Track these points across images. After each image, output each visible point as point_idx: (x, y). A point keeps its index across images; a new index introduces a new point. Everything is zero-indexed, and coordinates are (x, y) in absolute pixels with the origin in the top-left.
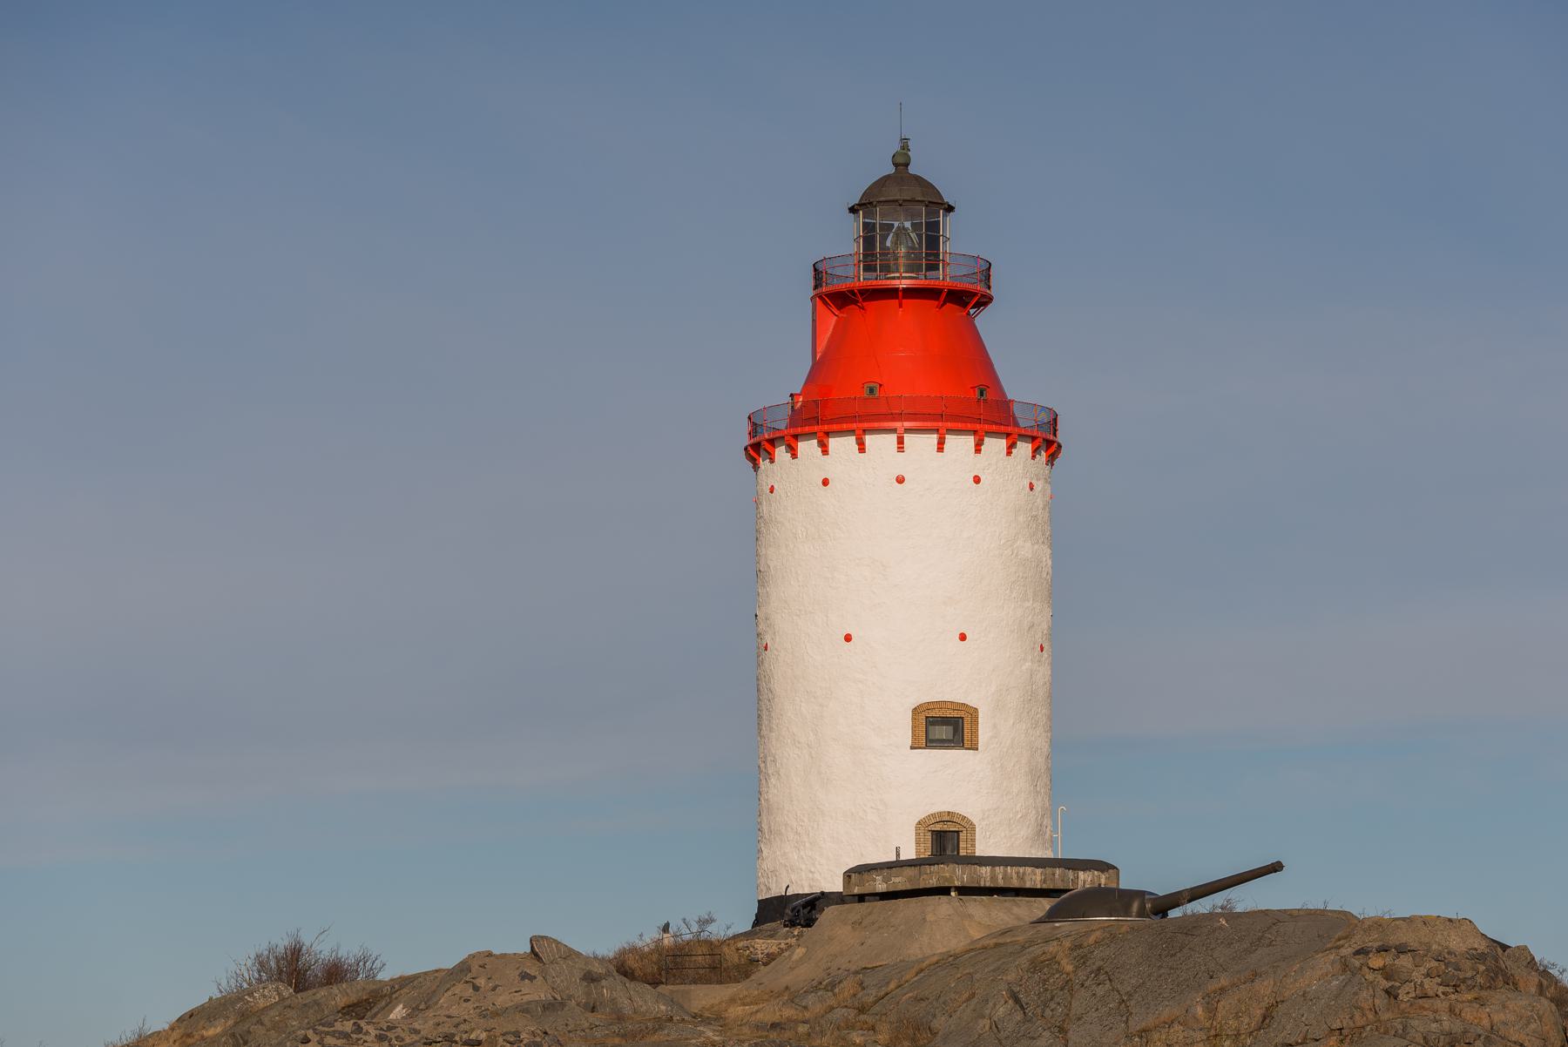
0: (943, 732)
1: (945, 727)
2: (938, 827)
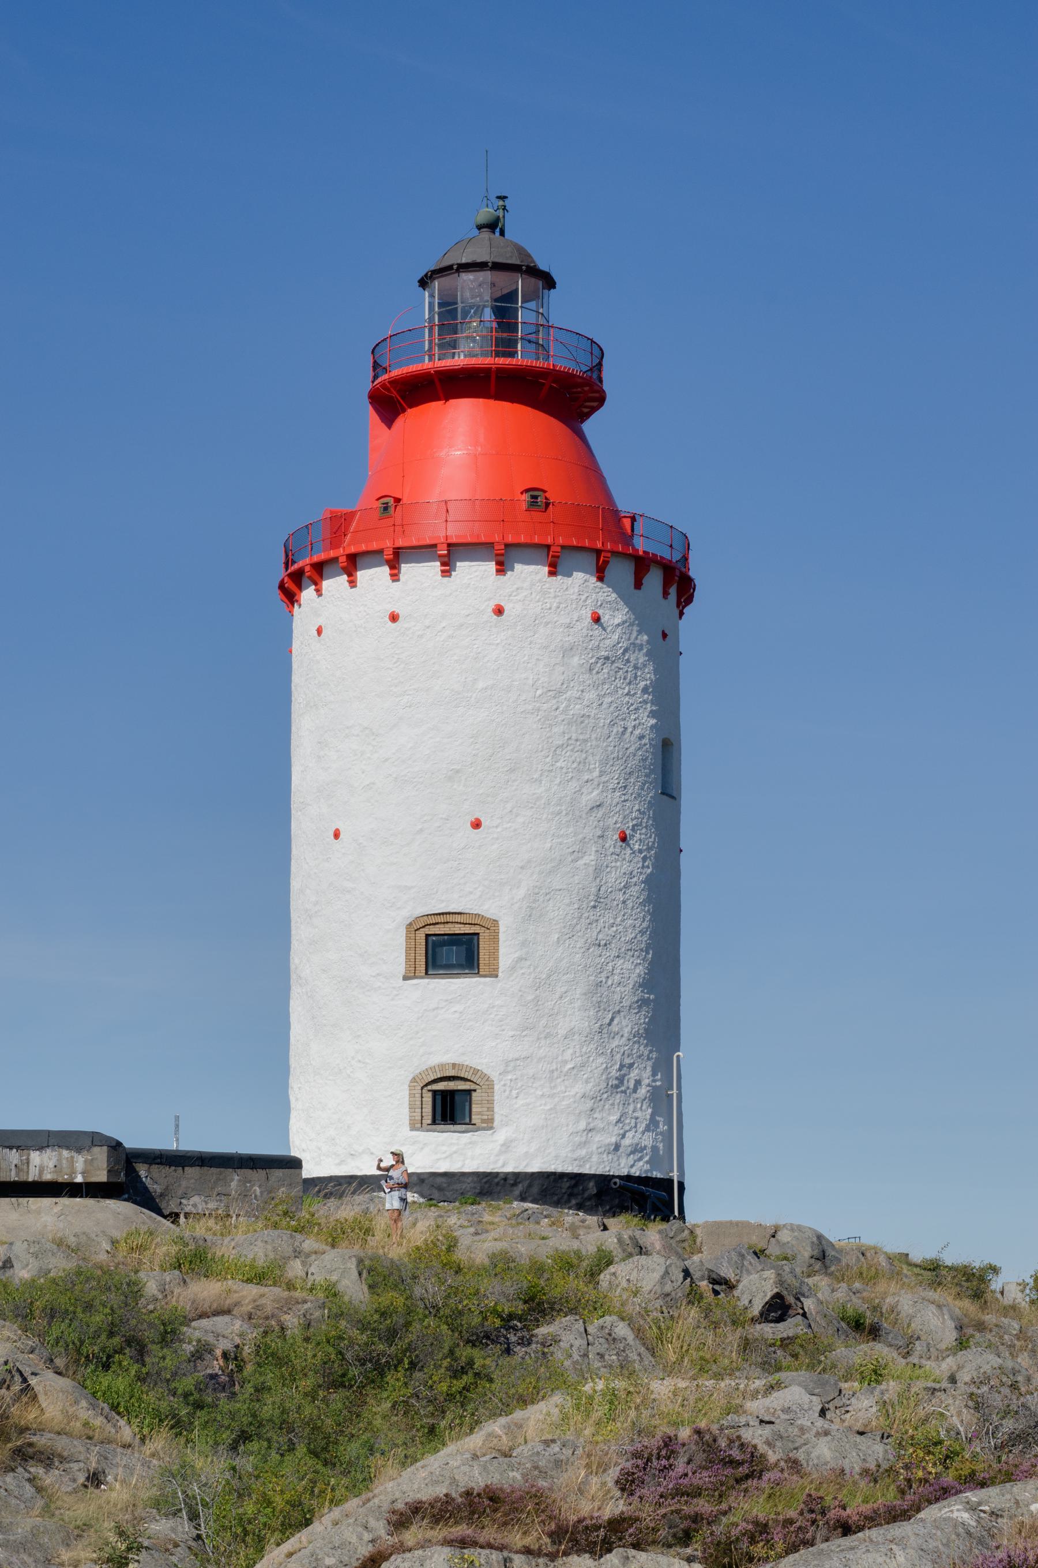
0: (453, 953)
1: (451, 949)
2: (441, 1086)
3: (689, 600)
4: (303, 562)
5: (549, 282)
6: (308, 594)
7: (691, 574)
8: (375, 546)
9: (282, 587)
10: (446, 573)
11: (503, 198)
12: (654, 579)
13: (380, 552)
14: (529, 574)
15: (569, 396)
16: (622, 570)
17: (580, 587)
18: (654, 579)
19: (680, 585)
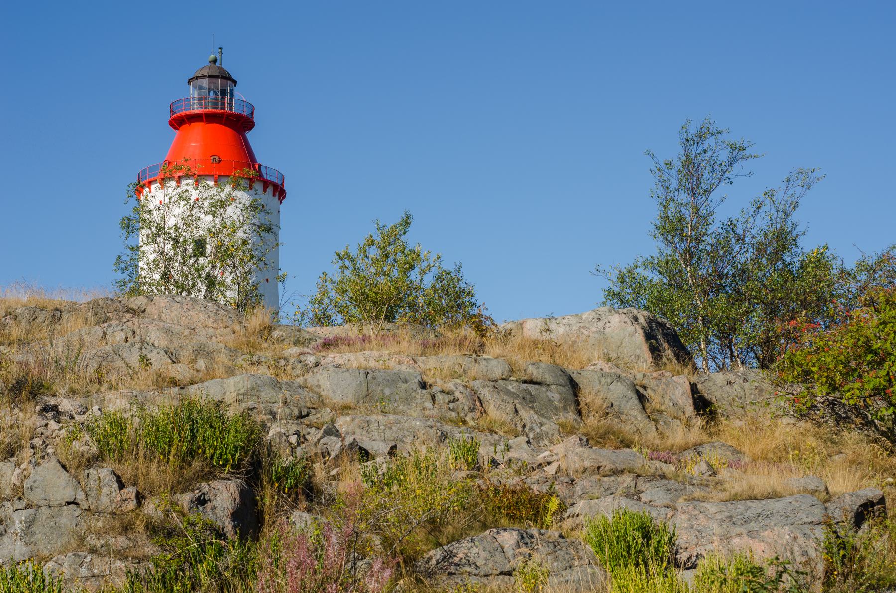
3: (284, 198)
5: (235, 82)
12: (270, 190)
15: (242, 124)
16: (258, 186)
18: (270, 190)
19: (280, 192)
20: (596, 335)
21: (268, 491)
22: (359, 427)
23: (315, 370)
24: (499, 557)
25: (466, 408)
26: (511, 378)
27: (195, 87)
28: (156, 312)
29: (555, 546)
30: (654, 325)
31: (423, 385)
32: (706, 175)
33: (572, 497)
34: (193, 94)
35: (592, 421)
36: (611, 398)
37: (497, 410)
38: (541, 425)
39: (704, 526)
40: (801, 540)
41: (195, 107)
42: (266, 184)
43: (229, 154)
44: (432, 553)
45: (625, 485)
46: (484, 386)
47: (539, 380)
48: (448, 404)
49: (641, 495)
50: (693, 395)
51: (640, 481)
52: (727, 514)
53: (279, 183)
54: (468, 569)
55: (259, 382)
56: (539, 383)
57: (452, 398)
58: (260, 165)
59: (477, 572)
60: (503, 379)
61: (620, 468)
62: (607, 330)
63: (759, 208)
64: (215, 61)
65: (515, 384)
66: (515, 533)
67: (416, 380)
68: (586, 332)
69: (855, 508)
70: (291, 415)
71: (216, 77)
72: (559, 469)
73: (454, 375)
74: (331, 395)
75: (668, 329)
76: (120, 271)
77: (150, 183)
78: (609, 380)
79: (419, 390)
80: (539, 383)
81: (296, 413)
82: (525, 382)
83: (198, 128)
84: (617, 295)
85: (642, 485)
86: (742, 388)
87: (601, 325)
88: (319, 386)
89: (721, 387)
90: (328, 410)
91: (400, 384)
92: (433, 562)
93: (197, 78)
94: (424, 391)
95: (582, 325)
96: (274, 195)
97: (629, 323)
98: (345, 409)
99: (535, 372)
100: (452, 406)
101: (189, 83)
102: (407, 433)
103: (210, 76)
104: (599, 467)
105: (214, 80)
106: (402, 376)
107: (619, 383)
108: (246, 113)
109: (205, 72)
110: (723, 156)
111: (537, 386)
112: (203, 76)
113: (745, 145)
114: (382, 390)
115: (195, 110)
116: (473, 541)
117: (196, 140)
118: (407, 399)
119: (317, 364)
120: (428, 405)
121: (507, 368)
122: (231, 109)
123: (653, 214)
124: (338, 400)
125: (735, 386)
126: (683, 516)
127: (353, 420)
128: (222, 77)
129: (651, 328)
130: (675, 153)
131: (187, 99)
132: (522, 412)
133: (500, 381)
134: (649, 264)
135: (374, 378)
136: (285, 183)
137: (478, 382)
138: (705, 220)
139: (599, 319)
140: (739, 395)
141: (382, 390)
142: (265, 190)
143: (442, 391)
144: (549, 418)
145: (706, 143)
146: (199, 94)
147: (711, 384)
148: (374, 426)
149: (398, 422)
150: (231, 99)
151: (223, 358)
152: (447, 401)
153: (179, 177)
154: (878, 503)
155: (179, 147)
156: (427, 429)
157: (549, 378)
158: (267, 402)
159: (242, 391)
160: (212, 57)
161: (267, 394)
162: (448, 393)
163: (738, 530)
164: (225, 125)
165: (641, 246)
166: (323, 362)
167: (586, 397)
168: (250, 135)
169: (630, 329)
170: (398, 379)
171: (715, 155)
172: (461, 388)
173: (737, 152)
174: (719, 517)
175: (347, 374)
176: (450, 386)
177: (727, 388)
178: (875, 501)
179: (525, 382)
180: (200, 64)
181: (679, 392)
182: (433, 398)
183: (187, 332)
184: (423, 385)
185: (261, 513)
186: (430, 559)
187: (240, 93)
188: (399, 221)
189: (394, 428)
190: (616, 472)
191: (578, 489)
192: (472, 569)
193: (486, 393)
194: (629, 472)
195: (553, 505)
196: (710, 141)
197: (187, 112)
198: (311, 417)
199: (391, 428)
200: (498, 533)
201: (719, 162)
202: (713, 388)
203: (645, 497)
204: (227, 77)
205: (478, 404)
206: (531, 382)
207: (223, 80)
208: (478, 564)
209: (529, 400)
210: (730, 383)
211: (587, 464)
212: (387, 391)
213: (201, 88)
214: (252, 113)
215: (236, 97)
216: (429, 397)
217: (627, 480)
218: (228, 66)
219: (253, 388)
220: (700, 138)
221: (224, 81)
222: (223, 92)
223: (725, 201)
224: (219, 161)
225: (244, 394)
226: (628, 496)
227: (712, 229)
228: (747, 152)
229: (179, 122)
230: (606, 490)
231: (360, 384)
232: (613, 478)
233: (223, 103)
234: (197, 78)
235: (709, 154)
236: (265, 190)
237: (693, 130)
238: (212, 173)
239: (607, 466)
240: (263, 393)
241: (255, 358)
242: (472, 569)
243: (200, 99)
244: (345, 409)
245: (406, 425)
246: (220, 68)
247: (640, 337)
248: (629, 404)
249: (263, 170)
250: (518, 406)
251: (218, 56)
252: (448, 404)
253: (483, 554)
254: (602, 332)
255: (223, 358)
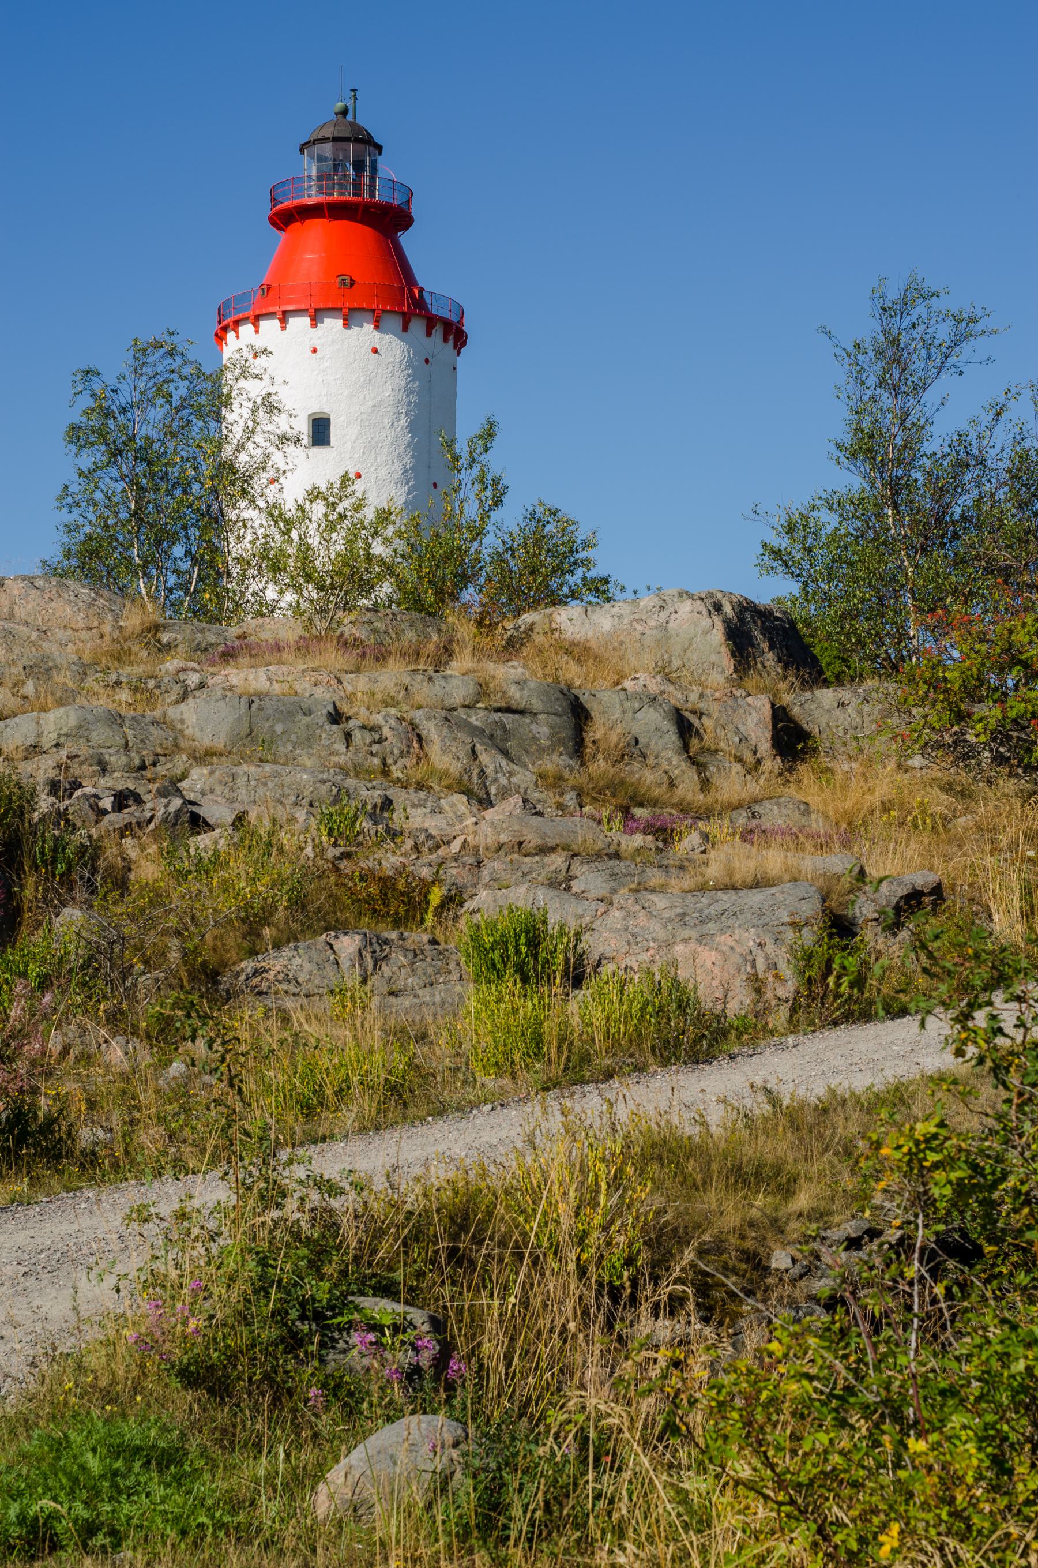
3: (464, 344)
4: (228, 321)
5: (379, 148)
6: (231, 335)
7: (465, 329)
8: (271, 309)
9: (216, 335)
10: (314, 325)
11: (354, 90)
12: (438, 332)
13: (275, 313)
14: (332, 324)
15: (390, 220)
16: (418, 326)
17: (366, 333)
18: (438, 332)
19: (455, 335)
20: (655, 632)
21: (31, 881)
22: (220, 782)
23: (197, 693)
24: (330, 971)
25: (396, 751)
26: (479, 705)
27: (311, 157)
28: (7, 603)
29: (416, 955)
30: (748, 615)
31: (336, 717)
32: (919, 364)
33: (475, 886)
34: (310, 168)
35: (600, 766)
36: (636, 729)
37: (444, 755)
38: (511, 774)
39: (642, 928)
40: (770, 948)
41: (313, 192)
42: (431, 322)
43: (368, 271)
44: (243, 965)
45: (553, 868)
46: (428, 719)
47: (521, 707)
48: (370, 745)
49: (572, 883)
50: (774, 725)
51: (576, 863)
52: (679, 910)
53: (455, 319)
54: (285, 987)
55: (90, 717)
56: (521, 712)
57: (377, 737)
58: (421, 290)
59: (296, 991)
60: (464, 706)
61: (551, 843)
62: (671, 625)
63: (998, 414)
64: (344, 112)
65: (482, 714)
66: (357, 937)
67: (325, 711)
68: (639, 628)
69: (894, 900)
70: (128, 765)
71: (347, 140)
72: (465, 844)
73: (390, 702)
74: (198, 734)
75: (777, 619)
76: (66, 510)
77: (237, 323)
78: (637, 706)
79: (327, 726)
80: (521, 712)
81: (137, 762)
82: (498, 710)
83: (316, 229)
84: (776, 553)
85: (577, 868)
86: (860, 712)
87: (663, 615)
88: (182, 721)
89: (829, 711)
90: (184, 757)
91: (300, 716)
92: (243, 977)
93: (315, 142)
94: (335, 727)
95: (637, 616)
96: (446, 340)
97: (705, 613)
98: (204, 757)
99: (516, 696)
100: (375, 748)
101: (302, 150)
102: (287, 791)
103: (335, 140)
104: (520, 843)
105: (343, 145)
106: (304, 706)
107: (651, 710)
108: (397, 200)
109: (328, 133)
110: (944, 332)
111: (517, 716)
112: (324, 140)
113: (979, 312)
114: (272, 727)
115: (313, 197)
116: (296, 948)
117: (315, 248)
118: (308, 739)
119: (202, 686)
120: (341, 747)
121: (472, 688)
122: (372, 195)
123: (839, 426)
124: (205, 741)
125: (850, 709)
126: (617, 914)
127: (212, 773)
128: (357, 140)
129: (741, 620)
130: (867, 328)
131: (299, 179)
132: (484, 758)
133: (460, 710)
134: (835, 505)
135: (260, 709)
136: (466, 321)
137: (421, 712)
138: (916, 432)
139: (662, 608)
140: (854, 724)
141: (272, 727)
142: (429, 334)
143: (364, 727)
144: (525, 766)
145: (915, 313)
146: (318, 170)
147: (813, 706)
148: (241, 781)
149: (278, 775)
150: (373, 179)
151: (65, 678)
152: (368, 741)
153: (284, 313)
154: (930, 894)
155: (286, 261)
156: (318, 785)
157: (537, 705)
158: (99, 746)
159: (65, 730)
160: (340, 105)
161: (100, 735)
162: (372, 729)
163: (686, 933)
164: (361, 222)
165: (821, 479)
166: (210, 682)
167: (596, 732)
168: (405, 239)
169: (706, 622)
170: (295, 708)
171: (930, 330)
172: (393, 722)
173: (966, 326)
174: (666, 914)
175: (222, 703)
176: (378, 719)
177: (837, 712)
178: (926, 891)
179: (498, 710)
180: (319, 116)
181: (752, 720)
182: (348, 736)
183: (34, 635)
184: (336, 717)
185: (18, 911)
186: (238, 974)
187: (388, 168)
188: (478, 432)
189: (270, 784)
190: (544, 850)
191: (485, 873)
192: (292, 988)
193: (430, 729)
194: (563, 849)
195: (436, 896)
196: (920, 310)
197: (297, 202)
198: (159, 768)
199: (265, 784)
200: (336, 937)
201: (937, 342)
202: (816, 712)
203: (576, 886)
204: (365, 141)
205: (416, 745)
206: (509, 710)
207: (357, 144)
208: (300, 980)
209: (499, 741)
210: (842, 705)
211: (503, 838)
212: (279, 728)
213: (321, 159)
214: (409, 202)
215: (380, 173)
216: (341, 735)
217: (557, 861)
218: (365, 120)
219: (80, 727)
220: (904, 306)
221: (361, 146)
222: (359, 166)
223: (947, 404)
224: (352, 285)
225: (67, 735)
226: (552, 884)
227: (928, 447)
228: (979, 327)
229: (285, 219)
230: (524, 875)
231: (239, 719)
232: (537, 858)
233: (357, 185)
234: (315, 142)
235: (920, 329)
236: (429, 334)
237: (893, 295)
238: (339, 305)
239: (533, 840)
240: (94, 734)
241: (113, 677)
242: (292, 988)
243: (320, 178)
244: (204, 757)
245: (288, 779)
246: (353, 125)
247: (718, 635)
248: (664, 740)
249: (427, 298)
250: (479, 748)
251: (350, 104)
252: (370, 745)
253: (307, 967)
254: (663, 628)
255: (65, 678)
